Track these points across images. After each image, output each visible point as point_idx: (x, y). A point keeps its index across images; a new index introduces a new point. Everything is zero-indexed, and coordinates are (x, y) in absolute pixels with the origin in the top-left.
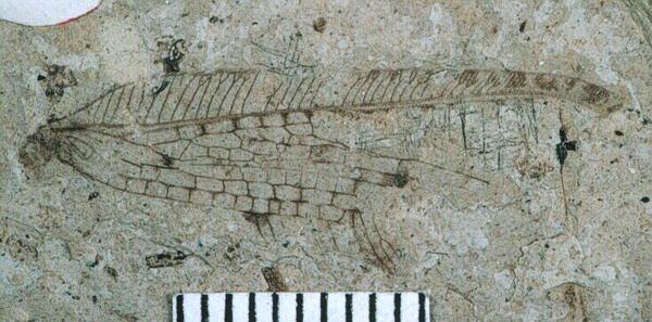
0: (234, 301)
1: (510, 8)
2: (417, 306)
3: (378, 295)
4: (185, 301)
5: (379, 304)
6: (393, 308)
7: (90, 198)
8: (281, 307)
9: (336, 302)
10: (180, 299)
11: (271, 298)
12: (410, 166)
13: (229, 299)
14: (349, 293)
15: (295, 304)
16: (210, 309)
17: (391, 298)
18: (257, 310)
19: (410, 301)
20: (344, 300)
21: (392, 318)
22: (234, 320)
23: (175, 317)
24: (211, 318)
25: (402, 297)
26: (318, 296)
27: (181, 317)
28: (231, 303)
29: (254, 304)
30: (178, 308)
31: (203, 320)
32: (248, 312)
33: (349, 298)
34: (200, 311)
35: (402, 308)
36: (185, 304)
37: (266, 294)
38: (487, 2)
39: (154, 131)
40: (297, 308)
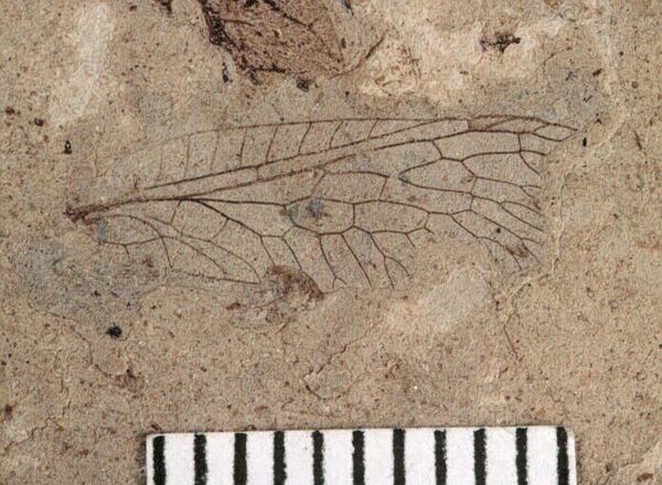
1: (332, 1)
2: (554, 449)
4: (167, 446)
5: (490, 447)
6: (513, 453)
7: (205, 370)
8: (327, 453)
10: (159, 444)
15: (351, 449)
19: (542, 442)
20: (432, 441)
21: (471, 478)
22: (408, 482)
23: (150, 473)
24: (212, 478)
26: (348, 435)
27: (160, 476)
28: (245, 449)
31: (477, 483)
32: (272, 463)
33: (440, 438)
34: (191, 463)
35: (529, 454)
40: (476, 465)
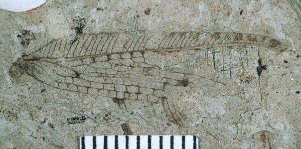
0: (108, 139)
1: (235, 3)
2: (193, 142)
3: (175, 137)
4: (85, 139)
5: (175, 141)
6: (181, 142)
7: (42, 92)
8: (130, 142)
9: (155, 140)
10: (83, 139)
11: (125, 138)
12: (189, 77)
13: (106, 138)
14: (161, 136)
15: (136, 141)
16: (97, 143)
17: (180, 138)
18: (119, 143)
19: (189, 139)
20: (159, 139)
21: (181, 147)
23: (81, 146)
24: (97, 147)
25: (186, 137)
26: (147, 137)
28: (107, 140)
29: (117, 141)
30: (82, 142)
32: (114, 144)
33: (161, 138)
34: (92, 144)
35: (185, 143)
36: (86, 141)
37: (123, 136)
38: (225, 1)
39: (71, 61)
40: (137, 143)
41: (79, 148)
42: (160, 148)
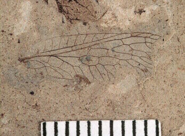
1: (93, 0)
2: (155, 126)
4: (47, 125)
5: (137, 125)
6: (143, 127)
7: (57, 104)
8: (91, 127)
10: (44, 125)
15: (98, 126)
19: (152, 124)
20: (121, 124)
23: (42, 133)
26: (97, 122)
28: (68, 126)
32: (76, 130)
33: (123, 123)
34: (54, 130)
35: (148, 127)
40: (133, 130)
41: (40, 135)
42: (111, 135)
